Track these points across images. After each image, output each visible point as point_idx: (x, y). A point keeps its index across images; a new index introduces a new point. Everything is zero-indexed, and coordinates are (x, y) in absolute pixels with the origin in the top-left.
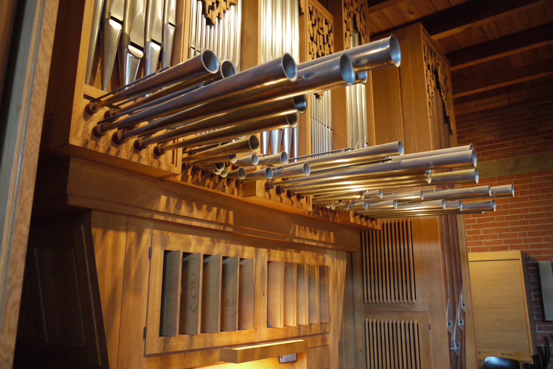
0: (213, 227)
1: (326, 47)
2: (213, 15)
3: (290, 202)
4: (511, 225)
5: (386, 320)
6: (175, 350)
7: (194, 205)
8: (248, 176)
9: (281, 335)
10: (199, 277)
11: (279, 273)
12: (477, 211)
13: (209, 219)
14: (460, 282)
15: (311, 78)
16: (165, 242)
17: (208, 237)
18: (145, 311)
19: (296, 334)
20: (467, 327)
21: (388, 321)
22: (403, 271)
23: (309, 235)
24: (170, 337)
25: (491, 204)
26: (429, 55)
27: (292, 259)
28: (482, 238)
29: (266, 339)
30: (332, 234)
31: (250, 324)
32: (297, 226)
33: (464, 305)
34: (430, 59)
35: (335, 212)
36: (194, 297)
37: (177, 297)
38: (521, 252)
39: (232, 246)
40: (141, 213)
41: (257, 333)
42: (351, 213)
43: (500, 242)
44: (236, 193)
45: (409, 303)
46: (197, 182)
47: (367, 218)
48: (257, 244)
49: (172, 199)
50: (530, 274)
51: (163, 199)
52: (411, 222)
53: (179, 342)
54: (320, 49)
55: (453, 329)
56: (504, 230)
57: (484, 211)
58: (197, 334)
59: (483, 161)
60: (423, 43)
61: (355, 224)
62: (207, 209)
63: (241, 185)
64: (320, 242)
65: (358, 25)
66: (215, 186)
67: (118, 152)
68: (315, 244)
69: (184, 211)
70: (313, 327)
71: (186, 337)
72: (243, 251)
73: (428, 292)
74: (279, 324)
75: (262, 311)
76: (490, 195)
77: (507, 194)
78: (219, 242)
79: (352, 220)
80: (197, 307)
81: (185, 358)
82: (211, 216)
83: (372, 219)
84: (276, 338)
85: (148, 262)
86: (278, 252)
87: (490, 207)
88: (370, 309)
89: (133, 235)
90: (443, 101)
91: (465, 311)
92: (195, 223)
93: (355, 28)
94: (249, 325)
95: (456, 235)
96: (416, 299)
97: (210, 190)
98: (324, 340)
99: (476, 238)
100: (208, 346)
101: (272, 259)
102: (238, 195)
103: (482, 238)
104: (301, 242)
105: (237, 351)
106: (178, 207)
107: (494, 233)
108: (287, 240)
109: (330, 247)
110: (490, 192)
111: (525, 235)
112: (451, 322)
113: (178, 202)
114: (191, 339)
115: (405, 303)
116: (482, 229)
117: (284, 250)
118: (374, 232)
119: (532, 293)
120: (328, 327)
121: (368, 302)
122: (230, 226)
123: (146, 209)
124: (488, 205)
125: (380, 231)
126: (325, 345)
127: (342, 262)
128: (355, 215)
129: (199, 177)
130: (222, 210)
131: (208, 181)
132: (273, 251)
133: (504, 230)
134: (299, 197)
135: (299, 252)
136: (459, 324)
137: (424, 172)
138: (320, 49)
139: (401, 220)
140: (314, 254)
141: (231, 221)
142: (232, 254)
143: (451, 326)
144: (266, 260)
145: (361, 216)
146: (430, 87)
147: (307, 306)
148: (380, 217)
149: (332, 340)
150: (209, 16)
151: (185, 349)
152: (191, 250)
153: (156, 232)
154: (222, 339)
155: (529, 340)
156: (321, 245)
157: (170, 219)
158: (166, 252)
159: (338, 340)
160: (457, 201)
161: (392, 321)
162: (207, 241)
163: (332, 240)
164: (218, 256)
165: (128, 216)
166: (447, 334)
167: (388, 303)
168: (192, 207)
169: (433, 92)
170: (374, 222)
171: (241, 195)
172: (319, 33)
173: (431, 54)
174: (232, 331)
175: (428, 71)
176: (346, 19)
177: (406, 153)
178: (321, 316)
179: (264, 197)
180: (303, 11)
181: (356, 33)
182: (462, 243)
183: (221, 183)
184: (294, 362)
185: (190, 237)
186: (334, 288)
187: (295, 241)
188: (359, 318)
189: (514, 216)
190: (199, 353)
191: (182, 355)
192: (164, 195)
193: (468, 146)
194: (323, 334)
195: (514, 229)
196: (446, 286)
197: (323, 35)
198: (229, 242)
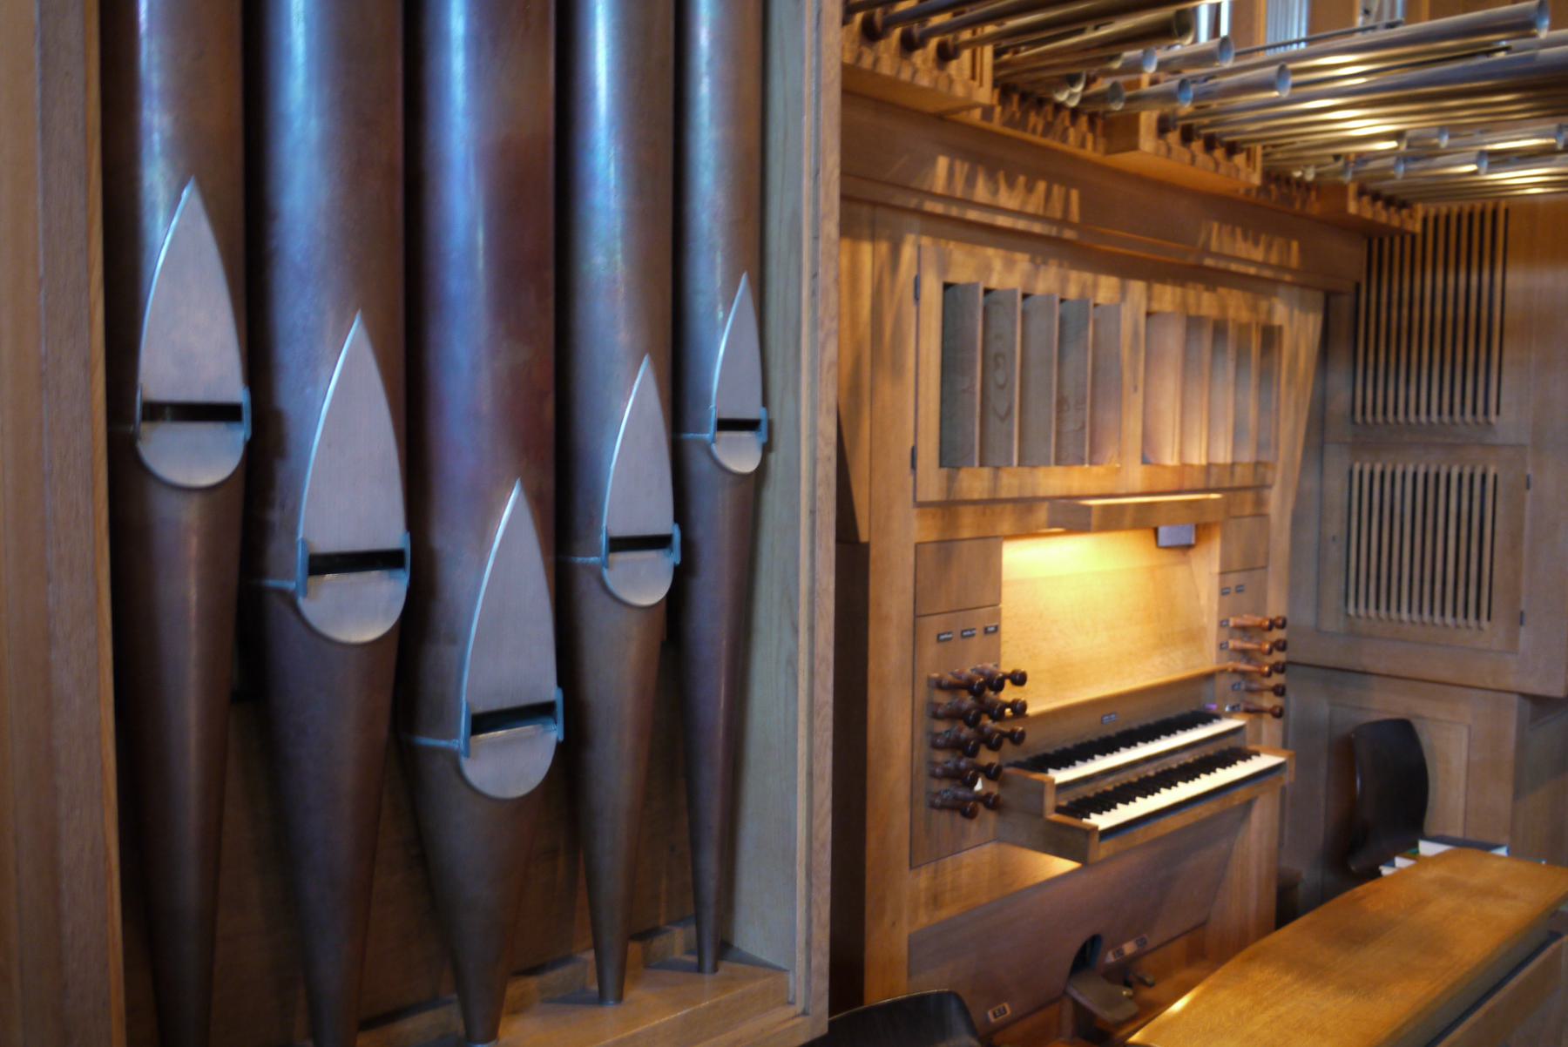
0: (1037, 228)
3: (1212, 166)
5: (1412, 464)
6: (968, 497)
8: (1130, 100)
9: (1168, 481)
11: (1172, 339)
13: (1030, 209)
16: (944, 265)
18: (912, 413)
19: (1199, 482)
23: (1243, 248)
24: (958, 468)
27: (1199, 306)
30: (1295, 245)
31: (1110, 452)
32: (1216, 225)
36: (1002, 387)
37: (973, 386)
39: (1074, 275)
40: (900, 199)
41: (1120, 475)
42: (1352, 189)
44: (1089, 144)
45: (1477, 423)
46: (1010, 122)
47: (1389, 202)
48: (1126, 269)
49: (958, 163)
51: (942, 163)
52: (1507, 211)
53: (975, 482)
58: (1010, 465)
61: (1358, 218)
63: (1099, 123)
64: (1264, 264)
66: (1048, 129)
67: (876, 61)
68: (1252, 271)
69: (981, 192)
70: (1238, 470)
71: (986, 471)
72: (1095, 286)
74: (1170, 458)
75: (1133, 426)
78: (1045, 263)
79: (1352, 208)
80: (1010, 408)
81: (984, 513)
82: (1034, 204)
84: (1160, 488)
88: (1368, 433)
89: (884, 247)
92: (1002, 221)
96: (1498, 412)
97: (1037, 139)
98: (1260, 502)
100: (1028, 493)
101: (1156, 307)
102: (1095, 148)
104: (1222, 264)
105: (1089, 508)
106: (970, 182)
108: (1191, 260)
109: (1288, 278)
114: (996, 478)
115: (1466, 423)
120: (1269, 475)
122: (1071, 226)
123: (913, 190)
126: (1260, 514)
128: (1361, 192)
130: (1056, 189)
132: (1157, 288)
134: (1232, 149)
139: (1478, 205)
140: (1249, 295)
141: (1075, 215)
142: (1073, 292)
144: (1143, 310)
145: (1376, 196)
147: (1230, 420)
148: (1423, 200)
149: (1277, 502)
151: (985, 496)
152: (994, 283)
153: (926, 241)
154: (1054, 481)
156: (1267, 273)
157: (954, 211)
158: (947, 286)
159: (1289, 506)
162: (1023, 261)
163: (1294, 261)
164: (1048, 296)
165: (874, 204)
168: (996, 182)
170: (1405, 212)
171: (1101, 147)
174: (1074, 464)
177: (1552, 27)
178: (1260, 447)
179: (1157, 153)
183: (1058, 121)
184: (1189, 547)
185: (990, 252)
186: (1289, 382)
187: (1209, 262)
188: (1337, 462)
190: (1009, 507)
191: (980, 508)
192: (943, 154)
194: (1259, 488)
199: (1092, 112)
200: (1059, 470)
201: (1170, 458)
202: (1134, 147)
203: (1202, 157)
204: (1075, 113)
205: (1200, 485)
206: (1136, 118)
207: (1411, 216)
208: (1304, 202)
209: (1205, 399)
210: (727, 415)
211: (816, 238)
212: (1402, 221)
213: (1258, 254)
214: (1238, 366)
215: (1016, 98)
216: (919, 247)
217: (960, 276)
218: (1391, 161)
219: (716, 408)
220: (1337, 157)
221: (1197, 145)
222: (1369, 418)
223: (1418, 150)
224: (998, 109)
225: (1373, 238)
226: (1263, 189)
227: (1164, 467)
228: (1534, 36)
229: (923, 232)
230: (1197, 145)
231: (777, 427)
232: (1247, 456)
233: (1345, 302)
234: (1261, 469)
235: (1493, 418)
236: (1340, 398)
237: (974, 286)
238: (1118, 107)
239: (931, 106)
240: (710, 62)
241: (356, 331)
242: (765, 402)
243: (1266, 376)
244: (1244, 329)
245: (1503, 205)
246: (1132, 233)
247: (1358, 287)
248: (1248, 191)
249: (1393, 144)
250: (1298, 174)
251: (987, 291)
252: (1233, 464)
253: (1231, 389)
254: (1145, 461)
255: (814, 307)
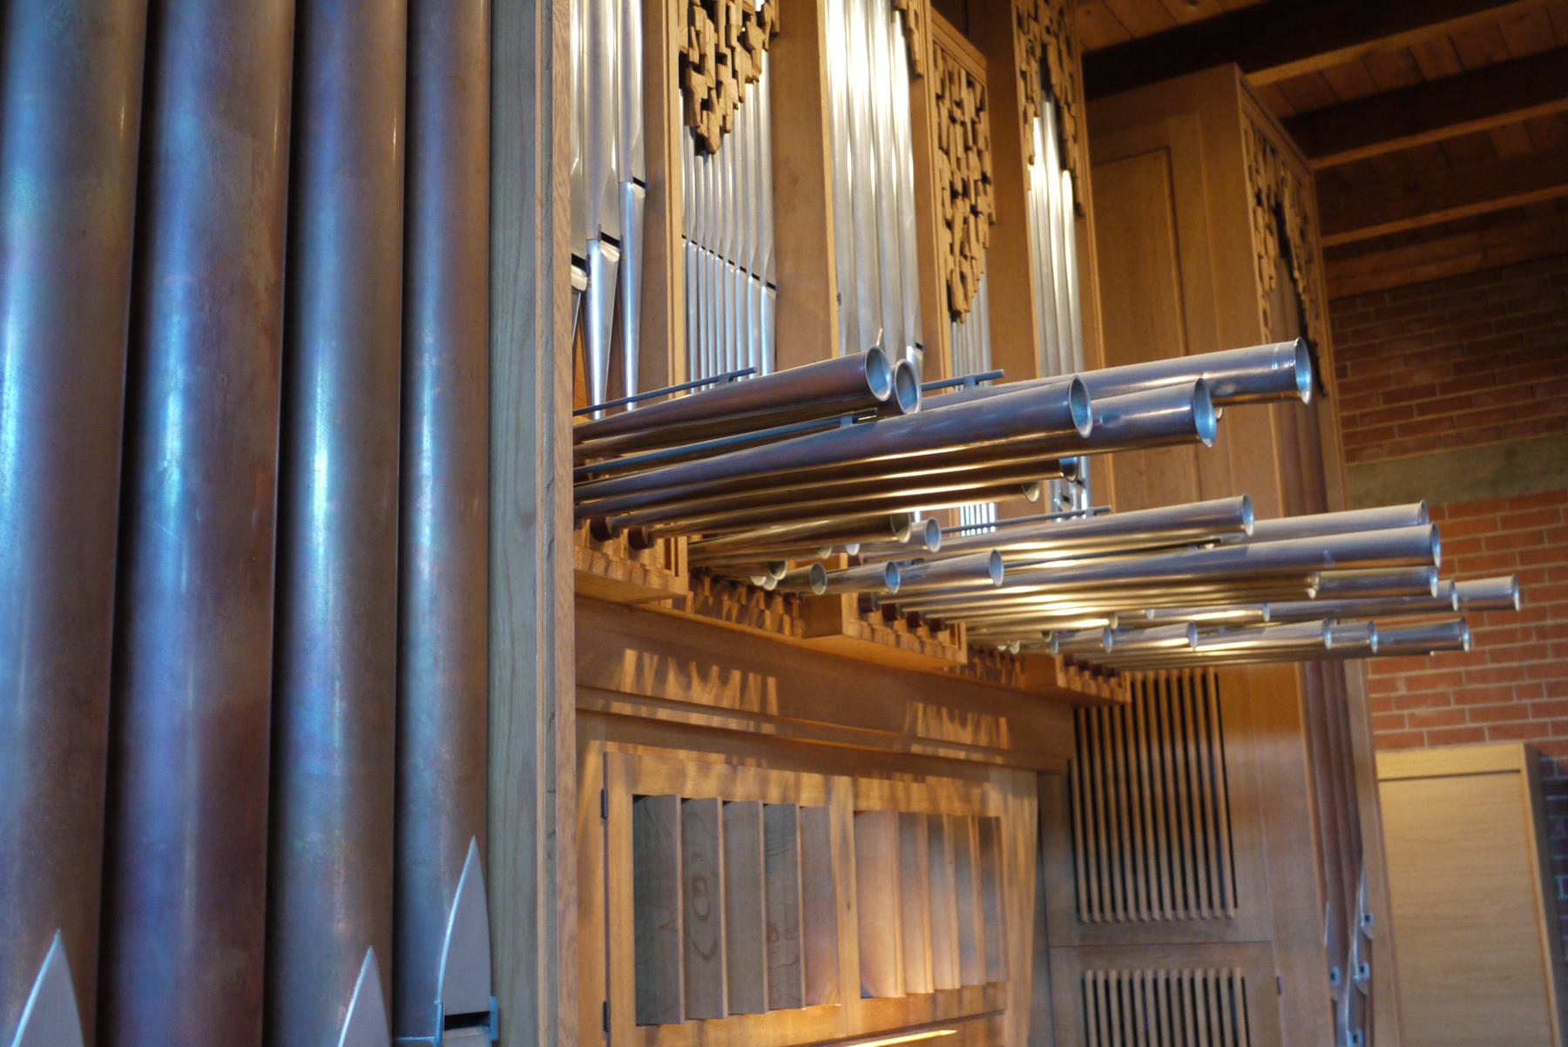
0: (733, 724)
1: (973, 156)
2: (710, 125)
3: (917, 646)
4: (1494, 660)
5: (1148, 969)
7: (693, 667)
8: (833, 582)
9: (891, 1018)
10: (716, 864)
11: (885, 842)
12: (1414, 651)
13: (725, 703)
14: (1356, 851)
15: (1111, 425)
16: (633, 776)
17: (717, 751)
19: (926, 1017)
20: (1379, 986)
21: (1156, 973)
22: (1196, 825)
23: (950, 730)
24: (658, 1025)
25: (1456, 631)
26: (1260, 158)
27: (909, 800)
28: (1402, 703)
29: (859, 1032)
30: (1003, 721)
31: (828, 988)
32: (920, 707)
33: (1367, 918)
34: (1262, 170)
35: (1022, 658)
36: (704, 918)
37: (674, 921)
38: (1528, 748)
39: (774, 774)
42: (1059, 661)
43: (1458, 717)
44: (787, 628)
45: (1215, 918)
47: (1097, 671)
48: (829, 762)
49: (646, 656)
50: (1552, 817)
51: (630, 656)
52: (1216, 676)
54: (959, 168)
55: (1341, 988)
56: (1472, 677)
57: (1435, 649)
58: (719, 1016)
59: (1405, 450)
60: (1244, 123)
62: (720, 677)
63: (796, 603)
64: (974, 747)
65: (1055, 79)
68: (962, 755)
70: (966, 995)
72: (798, 786)
73: (1270, 883)
74: (893, 990)
75: (849, 953)
76: (1456, 606)
77: (1498, 607)
78: (742, 763)
79: (1061, 681)
80: (716, 945)
83: (1112, 673)
84: (883, 1027)
85: (601, 829)
86: (876, 783)
87: (1455, 638)
90: (1298, 295)
91: (1370, 936)
92: (696, 719)
93: (1047, 86)
94: (827, 992)
95: (1343, 708)
96: (1236, 905)
97: (733, 625)
99: (1385, 704)
101: (863, 805)
102: (793, 633)
103: (1402, 703)
104: (930, 751)
106: (661, 677)
107: (1441, 689)
108: (897, 748)
110: (1455, 598)
111: (1535, 691)
112: (1336, 970)
113: (660, 662)
115: (1203, 918)
116: (1403, 674)
117: (889, 778)
118: (1105, 711)
119: (1560, 878)
121: (1092, 920)
124: (1445, 633)
125: (1123, 707)
127: (1026, 803)
128: (1068, 662)
129: (707, 593)
130: (751, 676)
131: (726, 601)
132: (863, 781)
133: (1472, 677)
134: (935, 626)
135: (923, 781)
136: (1357, 977)
137: (1305, 575)
138: (959, 168)
140: (959, 782)
141: (773, 708)
142: (774, 795)
143: (1337, 981)
144: (850, 809)
145: (1083, 666)
146: (1264, 261)
147: (955, 935)
148: (1133, 668)
150: (703, 130)
152: (689, 791)
153: (612, 747)
155: (1551, 1026)
157: (644, 712)
158: (637, 798)
159: (1025, 1034)
160: (1365, 622)
161: (1168, 973)
163: (1004, 741)
164: (750, 804)
166: (1329, 1004)
167: (1153, 920)
168: (688, 676)
169: (1273, 273)
170: (1113, 681)
171: (799, 631)
172: (953, 120)
173: (1264, 155)
175: (1259, 210)
176: (1024, 67)
178: (990, 963)
179: (861, 637)
180: (920, 69)
181: (1048, 99)
182: (1360, 732)
183: (753, 604)
185: (682, 754)
186: (1011, 880)
187: (916, 749)
188: (1067, 969)
189: (1502, 631)
192: (631, 647)
193: (1415, 508)
194: (990, 1014)
195: (1501, 675)
196: (1321, 863)
197: (963, 124)
198: (764, 762)
199: (792, 596)
200: (770, 1014)
201: (893, 991)
202: (838, 631)
203: (906, 636)
204: (770, 595)
205: (927, 1018)
206: (838, 597)
207: (1120, 685)
208: (1010, 675)
209: (926, 916)
210: (457, 1009)
211: (552, 791)
212: (1112, 692)
213: (966, 737)
214: (957, 870)
215: (707, 582)
216: (605, 755)
217: (653, 785)
218: (1099, 634)
219: (441, 1006)
220: (1045, 633)
221: (900, 624)
222: (1097, 916)
223: (1131, 624)
224: (691, 595)
225: (1080, 709)
226: (971, 665)
227: (888, 999)
228: (1244, 531)
229: (609, 737)
230: (900, 624)
231: (506, 1017)
232: (976, 978)
233: (1057, 782)
234: (991, 992)
235: (1231, 911)
236: (1062, 895)
237: (672, 797)
238: (820, 590)
239: (618, 596)
240: (434, 600)
241: (54, 953)
242: (493, 992)
243: (988, 878)
244: (959, 823)
245: (1211, 671)
246: (839, 726)
247: (1069, 763)
248: (952, 669)
249: (1105, 622)
250: (1002, 648)
251: (684, 800)
252: (960, 991)
253: (953, 898)
254: (865, 995)
255: (551, 873)
